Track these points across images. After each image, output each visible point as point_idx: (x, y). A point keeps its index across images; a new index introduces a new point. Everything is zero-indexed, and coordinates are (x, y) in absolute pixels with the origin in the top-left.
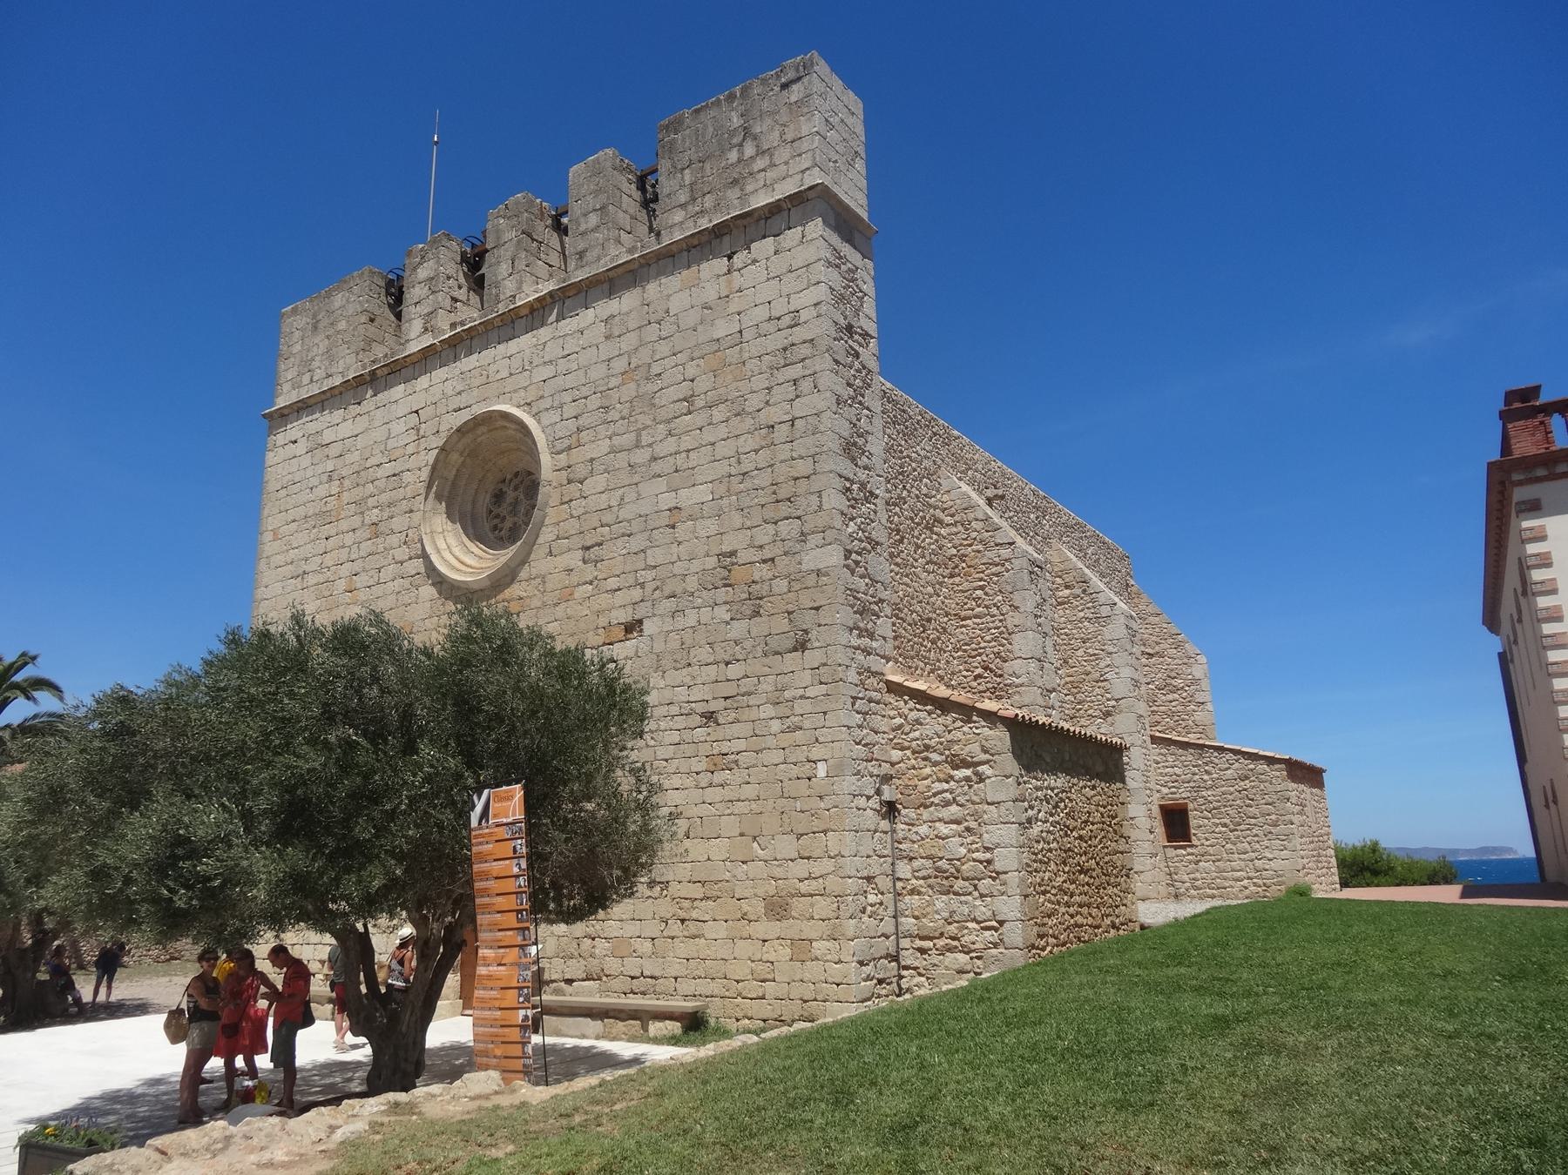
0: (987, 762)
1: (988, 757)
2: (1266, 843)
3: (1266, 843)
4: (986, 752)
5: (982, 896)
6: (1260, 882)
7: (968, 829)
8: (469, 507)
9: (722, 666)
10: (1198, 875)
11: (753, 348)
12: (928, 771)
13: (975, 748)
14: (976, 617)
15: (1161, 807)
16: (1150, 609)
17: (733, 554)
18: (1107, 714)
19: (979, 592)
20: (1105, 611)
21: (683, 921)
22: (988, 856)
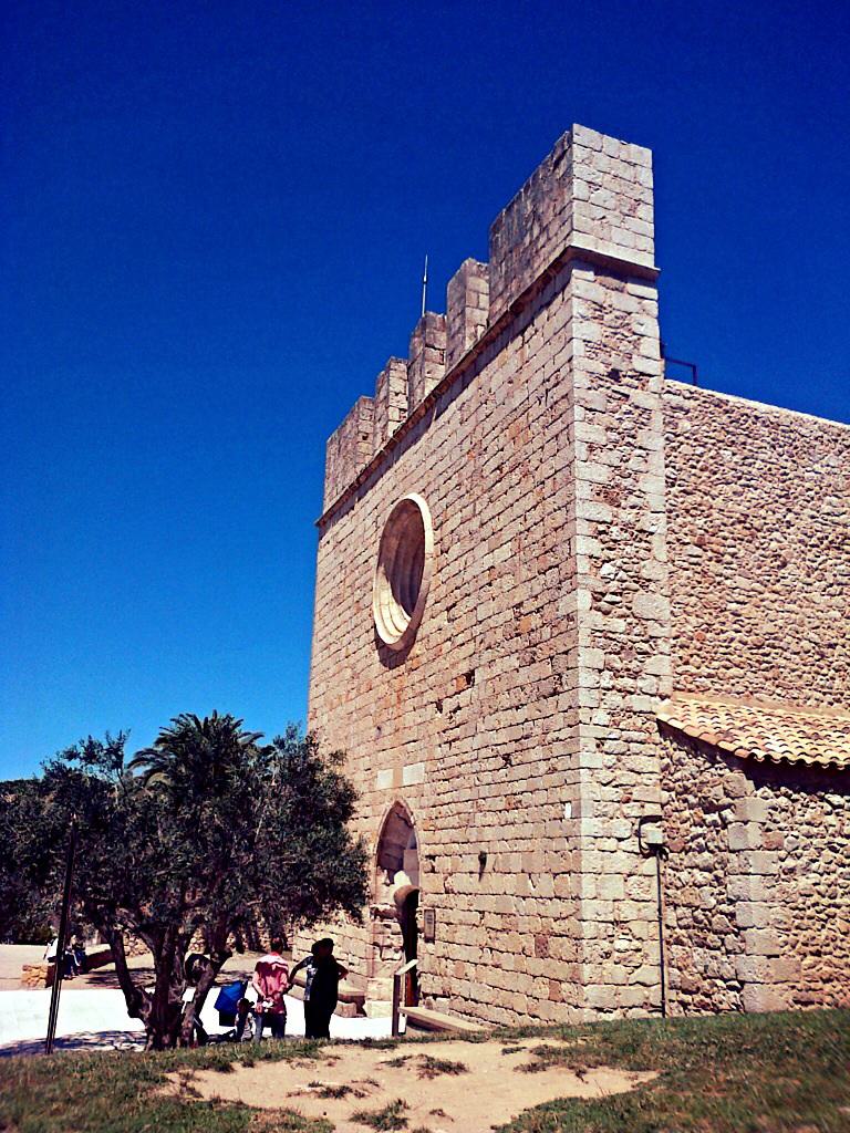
0: (728, 806)
1: (729, 800)
4: (727, 795)
7: (717, 878)
8: (407, 580)
9: (514, 709)
11: (534, 413)
12: (687, 813)
13: (719, 790)
17: (520, 605)
21: (491, 949)
22: (731, 908)
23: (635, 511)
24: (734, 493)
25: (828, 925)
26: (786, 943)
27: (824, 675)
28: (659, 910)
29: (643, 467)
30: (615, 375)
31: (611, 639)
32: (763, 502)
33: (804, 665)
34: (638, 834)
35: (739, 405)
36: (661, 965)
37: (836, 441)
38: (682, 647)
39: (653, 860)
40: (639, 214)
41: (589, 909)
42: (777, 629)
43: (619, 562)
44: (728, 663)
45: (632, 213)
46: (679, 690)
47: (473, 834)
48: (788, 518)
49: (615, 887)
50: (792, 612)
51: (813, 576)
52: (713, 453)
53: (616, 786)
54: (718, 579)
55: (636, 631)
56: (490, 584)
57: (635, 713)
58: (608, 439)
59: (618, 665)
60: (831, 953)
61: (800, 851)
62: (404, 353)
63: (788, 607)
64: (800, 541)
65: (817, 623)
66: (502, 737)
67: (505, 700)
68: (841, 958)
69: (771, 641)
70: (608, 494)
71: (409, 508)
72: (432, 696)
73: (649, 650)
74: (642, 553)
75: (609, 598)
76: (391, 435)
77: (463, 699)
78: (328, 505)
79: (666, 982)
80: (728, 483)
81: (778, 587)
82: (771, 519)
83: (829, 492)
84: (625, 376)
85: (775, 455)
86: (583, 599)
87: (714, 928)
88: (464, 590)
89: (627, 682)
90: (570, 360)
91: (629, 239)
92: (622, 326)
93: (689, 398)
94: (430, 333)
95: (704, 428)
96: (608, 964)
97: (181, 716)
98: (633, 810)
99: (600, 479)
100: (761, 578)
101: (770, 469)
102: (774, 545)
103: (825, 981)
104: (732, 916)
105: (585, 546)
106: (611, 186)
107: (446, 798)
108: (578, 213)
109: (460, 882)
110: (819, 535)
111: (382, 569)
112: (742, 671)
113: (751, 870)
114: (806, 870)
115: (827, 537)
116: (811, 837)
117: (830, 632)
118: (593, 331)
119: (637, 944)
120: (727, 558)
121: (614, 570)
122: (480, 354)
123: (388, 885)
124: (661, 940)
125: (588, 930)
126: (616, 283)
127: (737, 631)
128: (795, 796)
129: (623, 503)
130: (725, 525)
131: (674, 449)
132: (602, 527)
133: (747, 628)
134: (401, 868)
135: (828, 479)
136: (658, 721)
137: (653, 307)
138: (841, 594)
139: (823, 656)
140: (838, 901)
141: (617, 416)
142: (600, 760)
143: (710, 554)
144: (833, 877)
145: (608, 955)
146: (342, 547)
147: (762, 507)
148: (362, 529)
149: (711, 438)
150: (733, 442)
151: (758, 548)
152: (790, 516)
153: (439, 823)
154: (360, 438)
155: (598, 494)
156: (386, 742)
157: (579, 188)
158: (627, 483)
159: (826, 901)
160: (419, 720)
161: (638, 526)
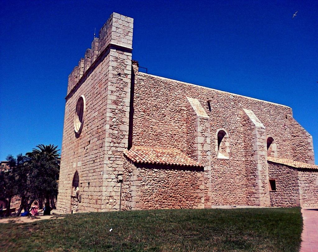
2: (293, 192)
3: (293, 192)
6: (291, 202)
7: (129, 187)
10: (277, 200)
14: (190, 133)
15: (269, 180)
16: (295, 123)
17: (98, 126)
18: (252, 155)
19: (190, 127)
20: (253, 127)
23: (122, 106)
24: (154, 99)
25: (151, 196)
26: (141, 200)
27: (172, 141)
28: (121, 194)
29: (125, 96)
30: (119, 74)
31: (113, 135)
32: (161, 102)
33: (168, 139)
34: (117, 178)
35: (157, 78)
36: (120, 205)
37: (181, 87)
38: (137, 136)
39: (120, 183)
40: (129, 35)
41: (104, 194)
42: (161, 131)
43: (117, 118)
44: (149, 139)
45: (127, 35)
46: (136, 145)
47: (88, 178)
48: (167, 105)
49: (111, 189)
50: (166, 127)
51: (172, 119)
52: (149, 90)
53: (112, 168)
54: (148, 120)
55: (120, 133)
56: (94, 121)
57: (118, 152)
58: (116, 90)
59: (115, 141)
60: (151, 201)
61: (146, 181)
62: (84, 58)
63: (165, 126)
64: (169, 111)
65: (172, 129)
66: (93, 156)
67: (95, 148)
68: (153, 202)
69: (160, 134)
70: (115, 103)
71: (81, 99)
72: (83, 146)
73: (123, 138)
74: (123, 116)
75: (114, 126)
76: (80, 78)
77: (88, 147)
78: (68, 93)
79: (121, 208)
80: (152, 97)
81: (163, 121)
82: (163, 105)
83: (178, 99)
84: (122, 75)
85: (165, 90)
86: (107, 127)
87: (128, 197)
88: (90, 121)
89: (117, 145)
90: (109, 71)
91: (125, 41)
92: (122, 63)
93: (144, 77)
94: (89, 54)
95: (147, 84)
96: (108, 205)
97: (39, 145)
98: (116, 173)
99: (114, 99)
100: (159, 119)
101: (163, 94)
102: (163, 112)
103: (149, 207)
104: (131, 194)
105: (109, 114)
106: (122, 28)
107: (84, 170)
108: (113, 35)
109: (86, 189)
110: (175, 109)
111: (77, 113)
112: (152, 141)
113: (134, 185)
114: (147, 185)
115: (176, 110)
116: (149, 178)
117: (175, 132)
118: (115, 64)
119: (115, 201)
120: (151, 115)
121: (115, 120)
122: (96, 64)
123: (75, 190)
124: (121, 200)
125: (103, 198)
126: (121, 52)
127: (151, 132)
128: (146, 170)
129: (119, 105)
130: (151, 107)
131: (139, 89)
132: (113, 110)
133: (154, 131)
134: (78, 186)
135: (178, 96)
136: (124, 153)
137: (131, 58)
138: (178, 123)
139: (172, 137)
140: (154, 191)
141: (119, 84)
142: (109, 162)
143: (146, 114)
144: (153, 186)
145: (108, 203)
146: (70, 106)
147: (161, 103)
148: (73, 102)
149: (149, 86)
150: (155, 87)
151: (159, 112)
152: (168, 105)
153: (83, 176)
154: (75, 78)
155: (113, 103)
156: (75, 156)
157: (114, 29)
158: (120, 100)
159: (151, 191)
160: (81, 151)
161: (122, 110)
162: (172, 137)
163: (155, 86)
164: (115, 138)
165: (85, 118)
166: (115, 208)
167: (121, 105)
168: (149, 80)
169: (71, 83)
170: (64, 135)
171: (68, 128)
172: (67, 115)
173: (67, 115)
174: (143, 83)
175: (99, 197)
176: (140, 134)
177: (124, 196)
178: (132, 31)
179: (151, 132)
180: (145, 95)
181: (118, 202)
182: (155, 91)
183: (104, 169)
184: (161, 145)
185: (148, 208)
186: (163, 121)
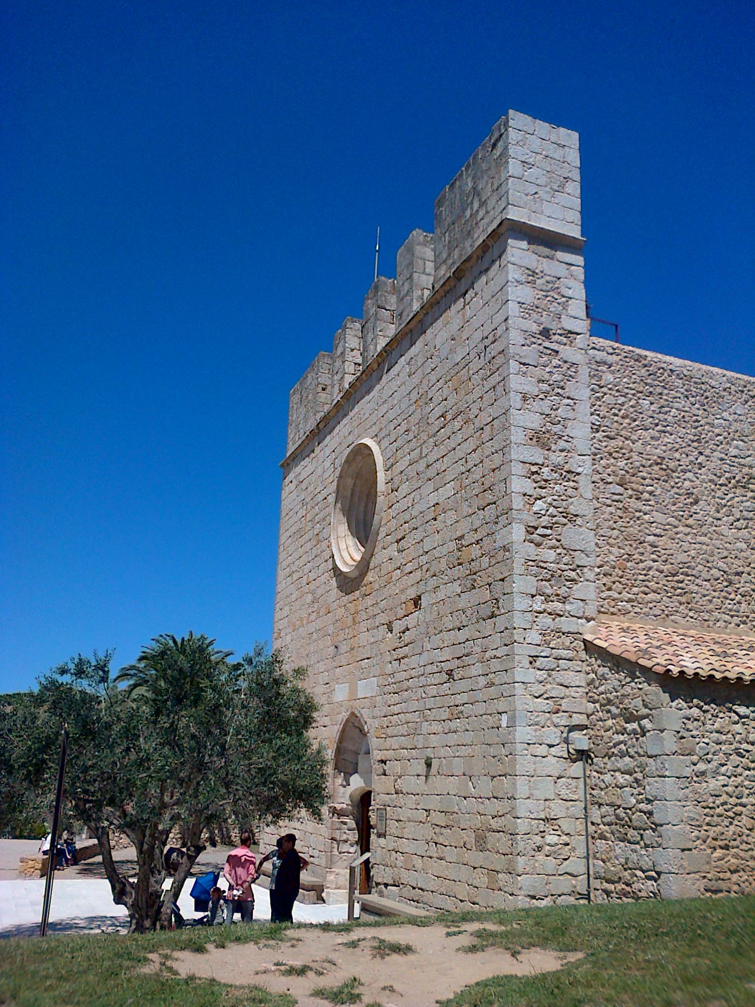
1: (647, 711)
4: (646, 706)
5: (647, 846)
7: (637, 780)
8: (362, 516)
9: (456, 630)
12: (610, 723)
13: (638, 702)
21: (436, 843)
22: (649, 807)
23: (564, 454)
25: (736, 822)
27: (732, 600)
28: (585, 808)
29: (571, 415)
30: (546, 333)
31: (542, 568)
32: (677, 446)
34: (566, 741)
35: (655, 360)
36: (587, 858)
37: (742, 391)
41: (523, 807)
43: (549, 500)
45: (561, 189)
46: (603, 613)
47: (420, 741)
48: (699, 461)
49: (547, 788)
50: (704, 544)
51: (722, 512)
53: (547, 699)
55: (565, 560)
56: (435, 519)
57: (564, 634)
59: (549, 591)
60: (737, 847)
61: (710, 756)
62: (358, 313)
63: (700, 539)
64: (710, 481)
65: (725, 553)
70: (539, 439)
71: (363, 451)
72: (383, 618)
74: (570, 492)
75: (540, 531)
76: (347, 386)
77: (411, 621)
79: (591, 873)
81: (691, 521)
82: (685, 461)
83: (736, 437)
84: (554, 334)
86: (518, 532)
87: (634, 825)
89: (557, 606)
93: (611, 354)
95: (625, 380)
96: (540, 857)
97: (161, 636)
98: (562, 720)
99: (533, 426)
100: (675, 514)
101: (683, 417)
103: (732, 872)
104: (650, 814)
105: (519, 485)
107: (396, 709)
108: (514, 190)
109: (410, 783)
110: (727, 475)
111: (339, 505)
112: (659, 597)
113: (667, 773)
114: (716, 773)
115: (734, 477)
117: (737, 562)
118: (527, 294)
119: (565, 838)
120: (646, 496)
125: (522, 826)
126: (546, 251)
127: (654, 561)
128: (706, 707)
129: (553, 447)
130: (644, 466)
131: (598, 399)
133: (664, 558)
137: (580, 273)
139: (731, 583)
140: (744, 800)
141: (547, 369)
142: (532, 675)
143: (630, 492)
145: (539, 849)
146: (304, 486)
147: (677, 450)
148: (320, 470)
151: (673, 487)
152: (701, 459)
155: (531, 439)
157: (514, 167)
158: (556, 429)
159: (733, 800)
160: (373, 640)
161: (566, 468)
162: (731, 583)
163: (651, 389)
164: (549, 580)
165: (385, 517)
166: (570, 872)
167: (562, 451)
168: (631, 366)
169: (303, 410)
170: (279, 588)
171: (301, 562)
172: (292, 521)
173: (292, 521)
174: (610, 377)
175: (492, 821)
176: (614, 568)
177: (607, 819)
178: (576, 175)
179: (652, 564)
180: (621, 420)
181: (579, 843)
182: (652, 408)
183: (517, 702)
184: (691, 614)
185: (728, 874)
186: (691, 521)
